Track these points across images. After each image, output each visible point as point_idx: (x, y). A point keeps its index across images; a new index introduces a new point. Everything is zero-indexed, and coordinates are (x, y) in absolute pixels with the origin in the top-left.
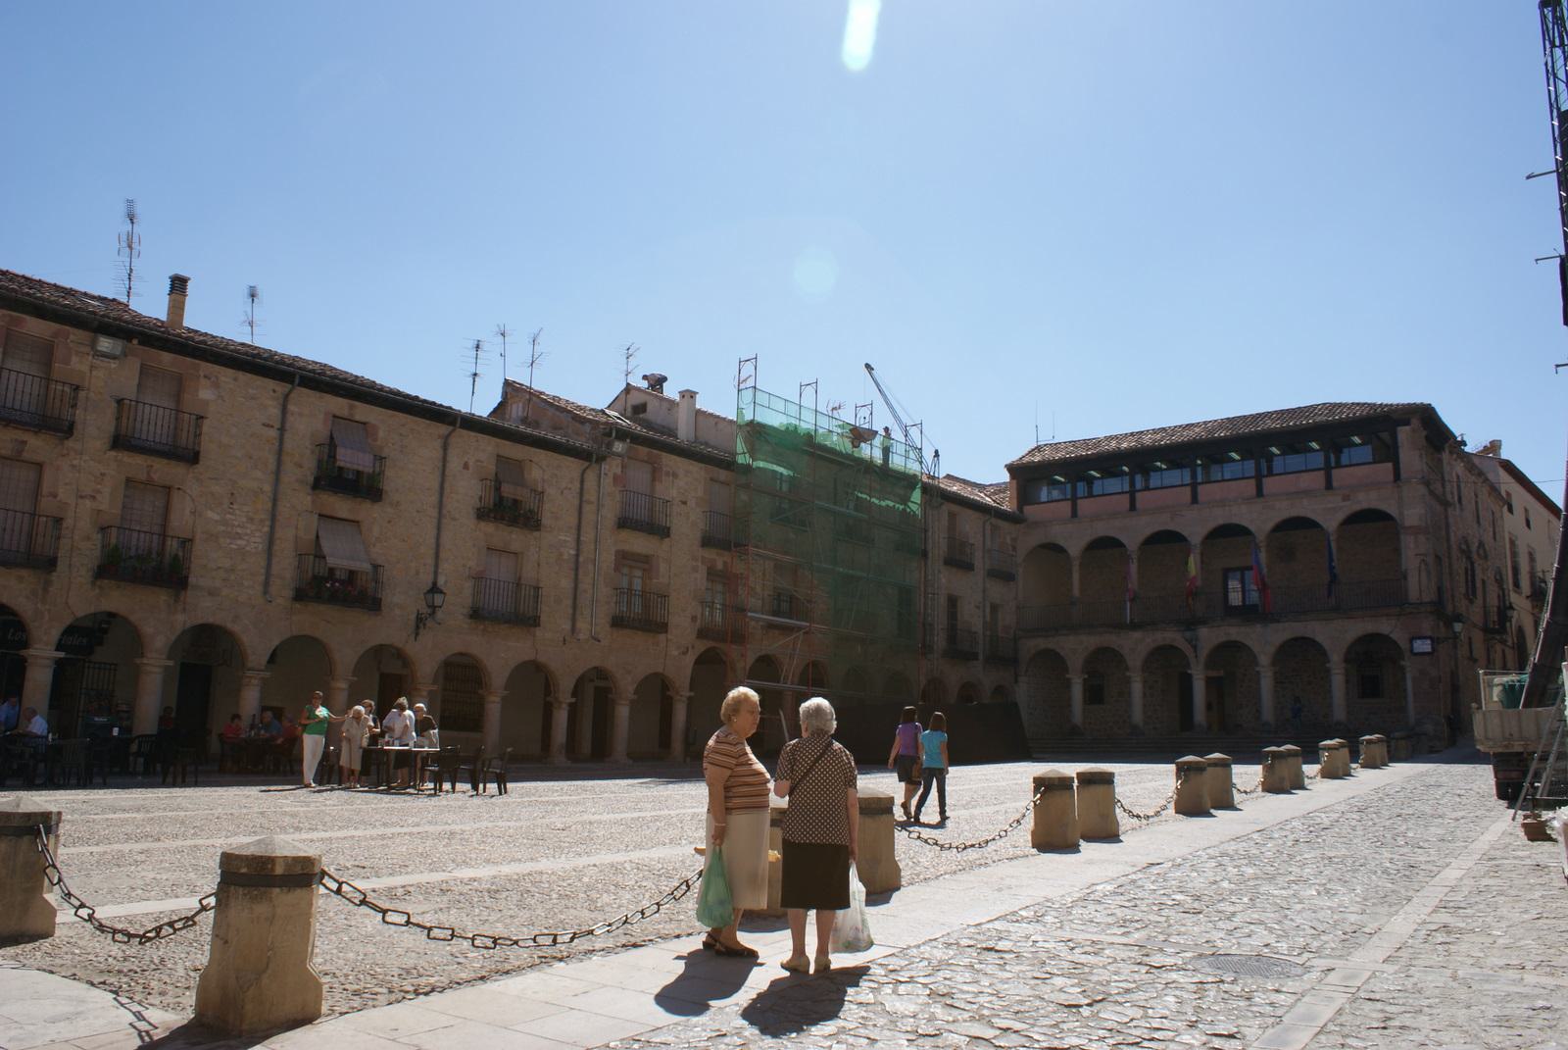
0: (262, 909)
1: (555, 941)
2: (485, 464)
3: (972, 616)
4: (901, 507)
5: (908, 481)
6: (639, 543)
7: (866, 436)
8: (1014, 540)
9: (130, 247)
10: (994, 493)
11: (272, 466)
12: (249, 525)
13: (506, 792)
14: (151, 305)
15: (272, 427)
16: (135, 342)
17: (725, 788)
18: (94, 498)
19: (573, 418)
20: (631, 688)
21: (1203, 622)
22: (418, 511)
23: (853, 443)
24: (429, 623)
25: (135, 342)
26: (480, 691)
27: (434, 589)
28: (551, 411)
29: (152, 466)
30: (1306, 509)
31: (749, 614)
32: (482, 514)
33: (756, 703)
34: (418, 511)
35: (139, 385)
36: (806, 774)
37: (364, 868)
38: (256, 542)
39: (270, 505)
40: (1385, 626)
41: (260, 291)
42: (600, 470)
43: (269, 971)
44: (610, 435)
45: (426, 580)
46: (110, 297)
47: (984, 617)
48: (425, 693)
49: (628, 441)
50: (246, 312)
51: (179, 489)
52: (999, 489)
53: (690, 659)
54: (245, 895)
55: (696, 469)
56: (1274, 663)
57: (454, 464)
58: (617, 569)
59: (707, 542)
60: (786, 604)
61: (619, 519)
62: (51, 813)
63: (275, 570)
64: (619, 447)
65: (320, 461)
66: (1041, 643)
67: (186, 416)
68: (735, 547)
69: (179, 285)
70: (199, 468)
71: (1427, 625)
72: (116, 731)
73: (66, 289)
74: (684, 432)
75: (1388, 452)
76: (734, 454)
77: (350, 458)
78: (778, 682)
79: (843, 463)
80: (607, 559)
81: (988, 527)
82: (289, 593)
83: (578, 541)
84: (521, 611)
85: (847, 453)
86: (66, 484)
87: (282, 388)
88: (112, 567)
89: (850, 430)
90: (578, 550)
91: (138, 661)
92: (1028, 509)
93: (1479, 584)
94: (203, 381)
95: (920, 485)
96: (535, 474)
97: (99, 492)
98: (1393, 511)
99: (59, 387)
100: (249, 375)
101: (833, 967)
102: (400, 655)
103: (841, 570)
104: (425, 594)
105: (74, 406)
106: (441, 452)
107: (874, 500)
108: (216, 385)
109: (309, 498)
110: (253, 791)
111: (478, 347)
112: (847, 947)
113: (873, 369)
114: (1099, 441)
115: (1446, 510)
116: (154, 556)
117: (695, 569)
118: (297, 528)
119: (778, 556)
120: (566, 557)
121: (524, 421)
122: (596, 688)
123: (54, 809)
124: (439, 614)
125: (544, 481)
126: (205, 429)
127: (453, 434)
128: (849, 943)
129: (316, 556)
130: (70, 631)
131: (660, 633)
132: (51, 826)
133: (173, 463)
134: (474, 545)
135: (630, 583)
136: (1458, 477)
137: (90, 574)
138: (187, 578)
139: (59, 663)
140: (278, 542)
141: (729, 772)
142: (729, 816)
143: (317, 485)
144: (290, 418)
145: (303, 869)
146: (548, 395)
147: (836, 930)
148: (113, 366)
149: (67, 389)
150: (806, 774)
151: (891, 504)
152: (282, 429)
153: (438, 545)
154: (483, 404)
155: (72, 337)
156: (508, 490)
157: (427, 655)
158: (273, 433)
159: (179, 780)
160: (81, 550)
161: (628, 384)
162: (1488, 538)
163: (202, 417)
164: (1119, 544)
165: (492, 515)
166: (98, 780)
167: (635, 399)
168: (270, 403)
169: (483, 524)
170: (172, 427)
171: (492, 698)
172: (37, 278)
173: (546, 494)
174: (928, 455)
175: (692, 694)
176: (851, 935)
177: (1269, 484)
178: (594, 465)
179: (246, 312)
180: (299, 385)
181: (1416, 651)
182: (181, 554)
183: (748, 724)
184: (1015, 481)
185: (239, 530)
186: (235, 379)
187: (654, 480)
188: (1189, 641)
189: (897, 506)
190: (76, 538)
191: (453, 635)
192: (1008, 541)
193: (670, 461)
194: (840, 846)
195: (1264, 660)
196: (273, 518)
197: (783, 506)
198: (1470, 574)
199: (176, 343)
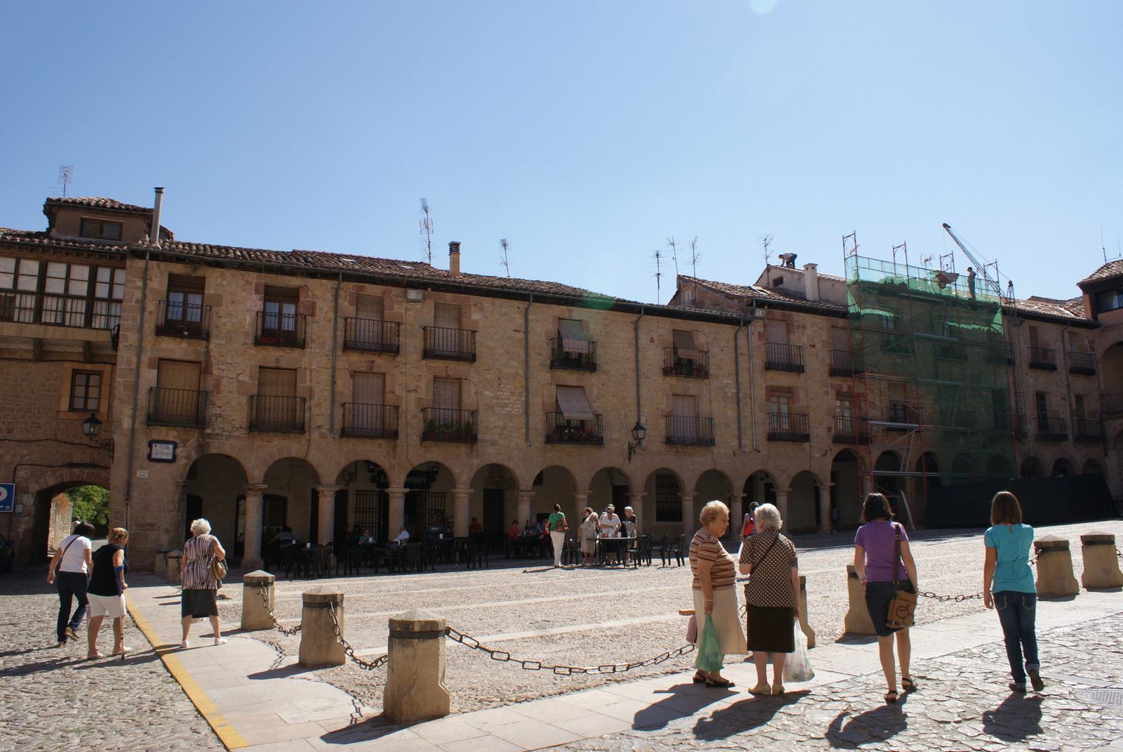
0: (409, 651)
1: (614, 670)
2: (665, 337)
3: (1059, 406)
4: (986, 329)
5: (991, 308)
6: (783, 379)
7: (949, 279)
8: (1092, 342)
9: (427, 228)
10: (1073, 306)
11: (522, 357)
12: (512, 398)
13: (684, 564)
14: (441, 263)
15: (520, 331)
16: (429, 289)
17: (712, 573)
18: (416, 391)
19: (726, 297)
20: (787, 483)
22: (622, 375)
23: (939, 285)
24: (638, 450)
25: (429, 289)
26: (679, 494)
27: (638, 427)
28: (711, 293)
29: (448, 367)
31: (870, 422)
32: (667, 372)
33: (726, 515)
34: (622, 375)
35: (435, 317)
36: (762, 559)
37: (549, 621)
38: (517, 408)
39: (524, 382)
41: (508, 242)
43: (415, 687)
44: (751, 305)
45: (632, 421)
46: (419, 262)
48: (639, 498)
49: (766, 307)
50: (501, 257)
51: (466, 379)
52: (1076, 303)
53: (829, 459)
54: (399, 643)
55: (819, 320)
57: (644, 340)
58: (768, 399)
59: (833, 372)
60: (901, 413)
61: (766, 363)
62: (337, 595)
63: (532, 425)
64: (759, 313)
65: (553, 350)
67: (465, 332)
68: (855, 374)
69: (454, 247)
70: (477, 364)
72: (441, 536)
73: (393, 261)
74: (811, 293)
76: (847, 306)
77: (573, 345)
78: (899, 470)
79: (935, 301)
80: (761, 393)
81: (1066, 335)
82: (542, 439)
83: (737, 382)
84: (701, 436)
85: (936, 294)
86: (400, 384)
87: (522, 305)
88: (431, 433)
89: (937, 276)
91: (453, 491)
92: (1101, 316)
94: (473, 308)
95: (1000, 310)
96: (701, 340)
97: (418, 387)
99: (389, 325)
100: (502, 300)
101: (785, 692)
102: (620, 472)
103: (940, 382)
104: (632, 431)
105: (398, 335)
106: (634, 333)
107: (963, 326)
108: (482, 310)
109: (549, 375)
110: (519, 571)
111: (658, 255)
112: (795, 678)
113: (949, 227)
116: (455, 423)
117: (827, 393)
118: (543, 396)
119: (888, 377)
120: (729, 395)
121: (693, 302)
123: (339, 592)
124: (644, 443)
125: (708, 343)
126: (478, 338)
127: (641, 320)
128: (796, 675)
129: (556, 413)
130: (413, 473)
131: (804, 442)
132: (337, 603)
133: (461, 363)
134: (663, 394)
135: (779, 409)
137: (419, 438)
138: (476, 435)
139: (406, 495)
140: (531, 406)
141: (713, 563)
142: (714, 592)
143: (552, 367)
144: (530, 324)
145: (431, 628)
147: (787, 666)
148: (419, 307)
149: (393, 325)
150: (762, 559)
151: (977, 327)
152: (526, 333)
153: (638, 397)
154: (663, 296)
155: (393, 293)
156: (683, 353)
157: (638, 472)
158: (520, 336)
159: (477, 565)
160: (412, 427)
161: (768, 265)
163: (475, 331)
165: (674, 372)
166: (429, 567)
167: (774, 275)
168: (517, 316)
169: (668, 379)
170: (457, 340)
171: (687, 498)
172: (376, 257)
173: (710, 353)
174: (1004, 287)
175: (833, 484)
176: (797, 670)
178: (743, 328)
179: (501, 257)
180: (534, 301)
181: (154, 456)
182: (471, 421)
183: (720, 527)
184: (1087, 295)
185: (506, 401)
186: (493, 304)
189: (982, 328)
190: (408, 417)
191: (656, 456)
192: (1086, 342)
193: (798, 317)
194: (789, 608)
196: (527, 390)
197: (890, 339)
199: (454, 286)
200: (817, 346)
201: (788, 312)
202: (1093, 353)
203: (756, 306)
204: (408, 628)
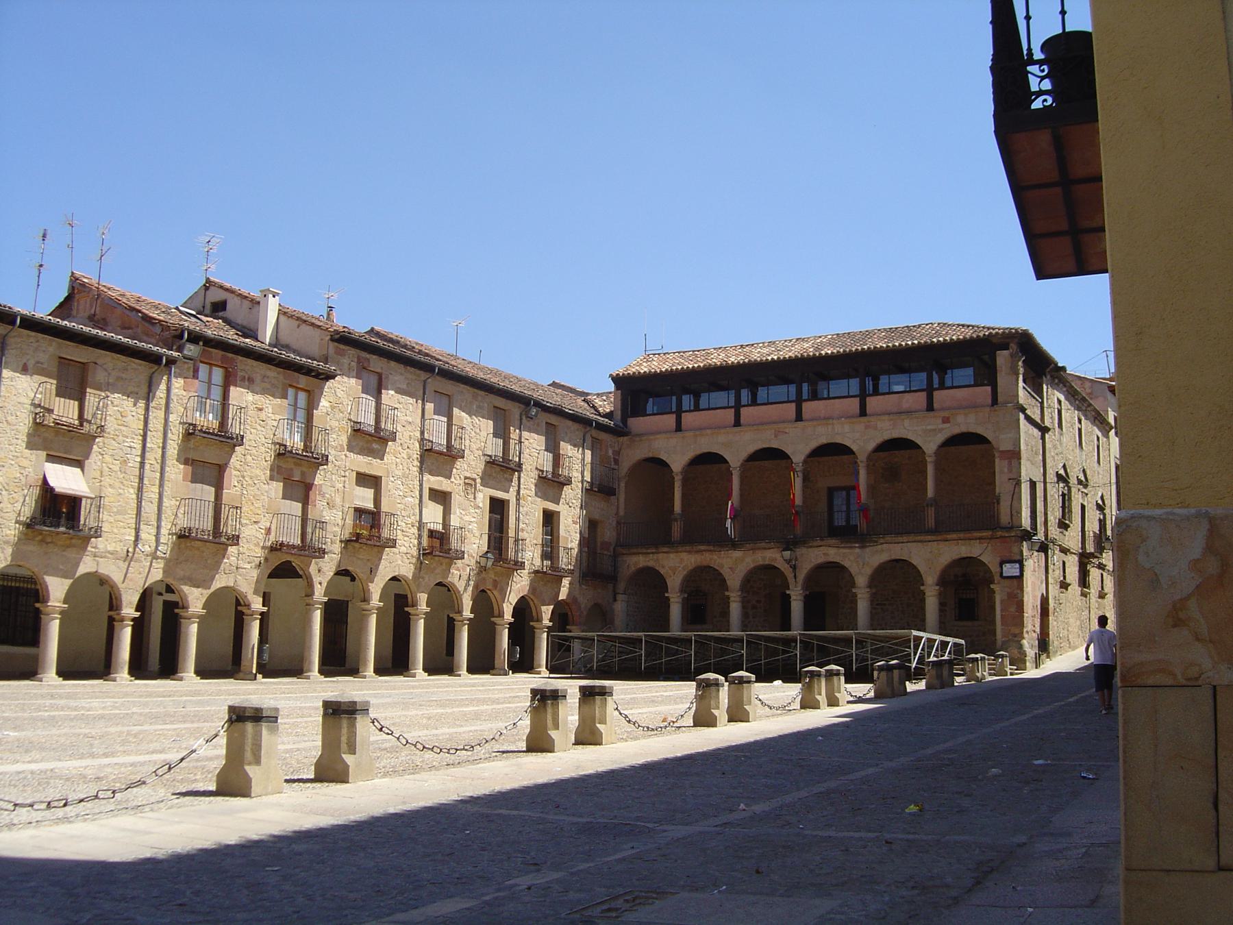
2: (45, 366)
8: (617, 453)
30: (907, 429)
44: (181, 336)
49: (201, 343)
56: (870, 586)
93: (1076, 510)
115: (1043, 438)
122: (166, 603)
164: (722, 460)
177: (873, 403)
181: (1004, 575)
188: (788, 561)
192: (610, 452)
195: (861, 581)
198: (1066, 499)
201: (230, 355)
202: (616, 467)
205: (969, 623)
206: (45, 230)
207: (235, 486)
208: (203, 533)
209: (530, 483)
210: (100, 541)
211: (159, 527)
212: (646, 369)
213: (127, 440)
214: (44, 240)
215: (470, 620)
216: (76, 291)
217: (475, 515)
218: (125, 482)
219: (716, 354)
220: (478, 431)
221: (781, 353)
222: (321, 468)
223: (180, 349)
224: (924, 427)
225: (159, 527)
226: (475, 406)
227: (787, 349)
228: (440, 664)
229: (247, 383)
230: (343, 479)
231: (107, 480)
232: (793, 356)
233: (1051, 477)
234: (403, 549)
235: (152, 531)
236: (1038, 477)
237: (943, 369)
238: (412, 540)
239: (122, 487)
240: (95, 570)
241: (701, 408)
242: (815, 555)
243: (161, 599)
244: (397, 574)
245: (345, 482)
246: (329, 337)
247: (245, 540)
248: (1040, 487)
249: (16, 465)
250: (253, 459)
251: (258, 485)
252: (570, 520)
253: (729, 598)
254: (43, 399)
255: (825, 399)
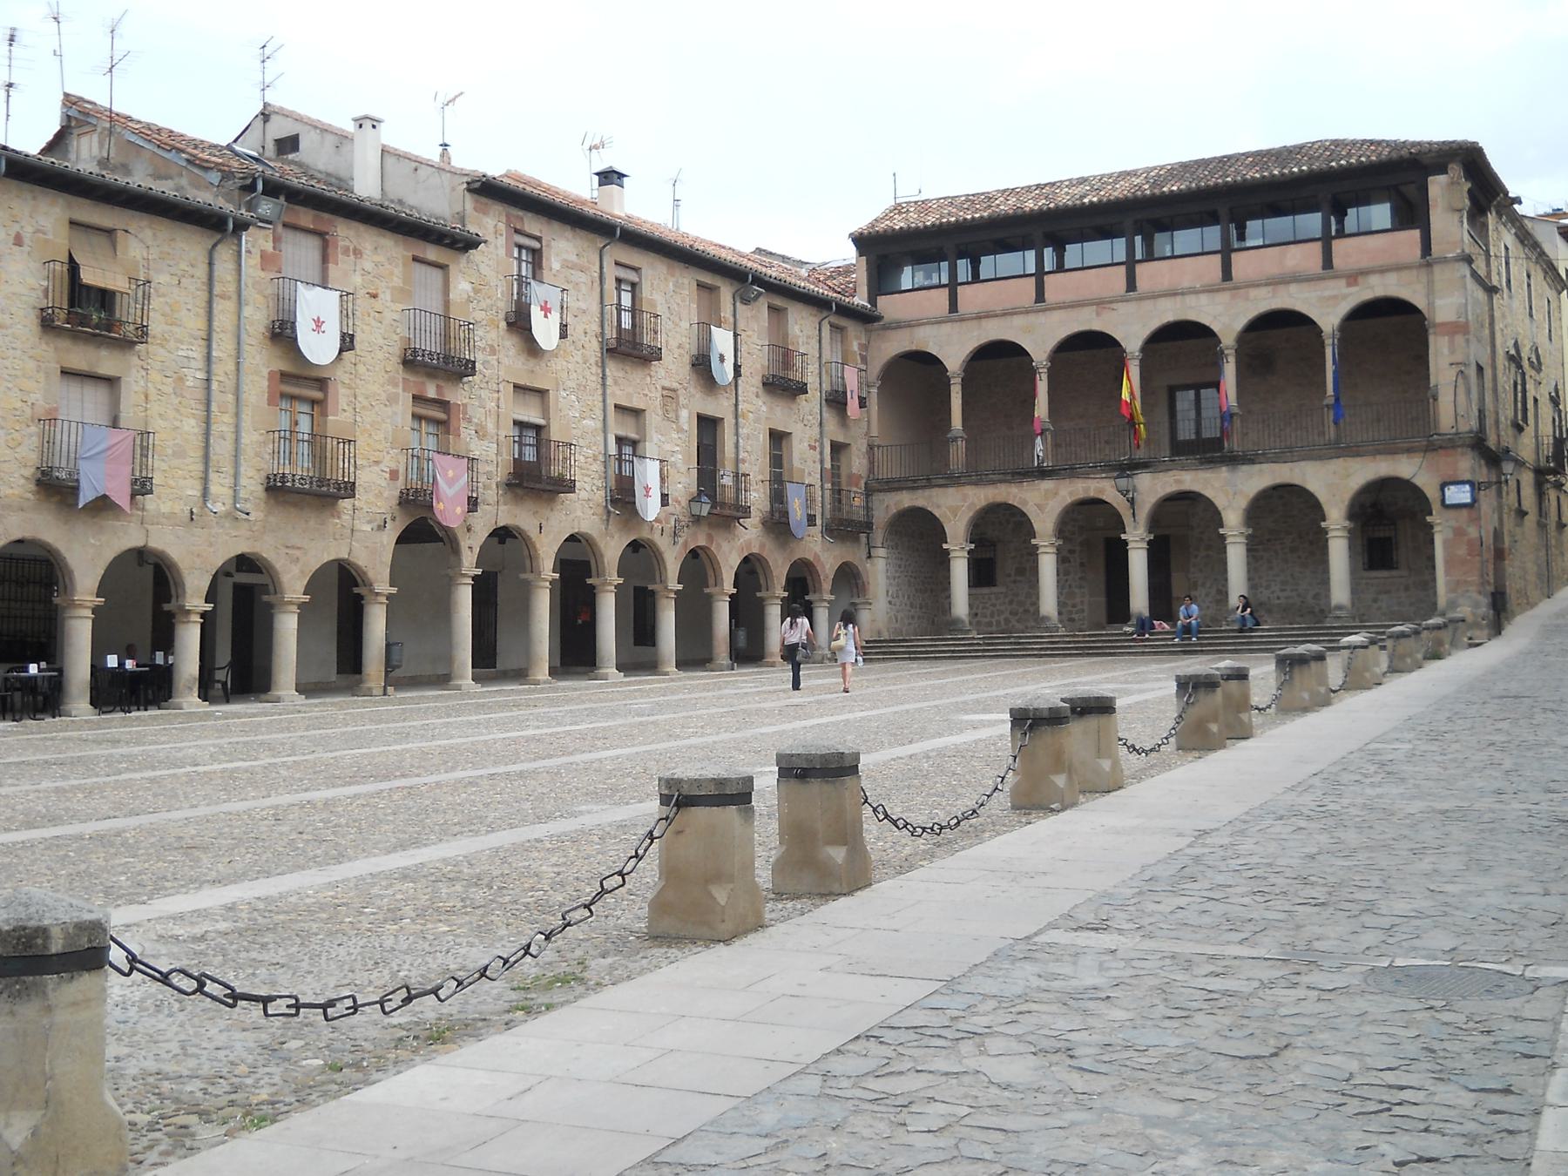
2: (50, 237)
21: (1144, 465)
40: (1405, 467)
42: (240, 245)
44: (251, 188)
47: (822, 462)
53: (389, 537)
66: (906, 500)
71: (1466, 464)
75: (1412, 214)
83: (208, 358)
90: (208, 372)
92: (882, 301)
98: (1420, 303)
114: (989, 198)
115: (1491, 299)
136: (1507, 248)
145: (90, 941)
146: (139, 122)
161: (266, 105)
162: (1542, 340)
181: (1448, 502)
187: (325, 259)
188: (1124, 493)
198: (1520, 388)
200: (381, 296)
203: (264, 193)
204: (28, 945)
205: (1385, 573)
206: (13, 29)
207: (344, 410)
208: (303, 482)
209: (750, 394)
210: (150, 499)
211: (236, 476)
212: (902, 225)
213: (182, 347)
214: (11, 45)
215: (677, 592)
216: (73, 124)
217: (679, 442)
218: (183, 410)
219: (1002, 199)
220: (677, 320)
221: (1102, 193)
222: (465, 379)
223: (251, 207)
224: (1319, 293)
225: (236, 476)
226: (671, 284)
227: (1110, 187)
228: (695, 656)
229: (352, 257)
230: (496, 395)
231: (155, 408)
232: (1121, 196)
233: (1501, 360)
234: (583, 495)
235: (227, 481)
236: (1485, 361)
237: (1339, 210)
238: (595, 482)
239: (179, 417)
240: (142, 544)
241: (1156, 256)
242: (1152, 487)
243: (230, 581)
244: (576, 530)
245: (498, 399)
246: (465, 186)
247: (362, 490)
248: (1488, 373)
249: (16, 390)
250: (368, 370)
251: (377, 408)
252: (806, 444)
253: (1127, 544)
254: (51, 287)
255: (1168, 258)
